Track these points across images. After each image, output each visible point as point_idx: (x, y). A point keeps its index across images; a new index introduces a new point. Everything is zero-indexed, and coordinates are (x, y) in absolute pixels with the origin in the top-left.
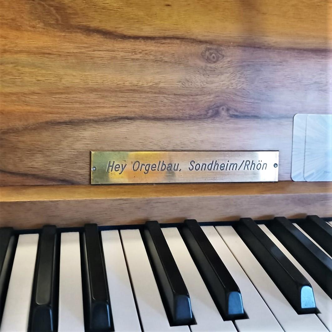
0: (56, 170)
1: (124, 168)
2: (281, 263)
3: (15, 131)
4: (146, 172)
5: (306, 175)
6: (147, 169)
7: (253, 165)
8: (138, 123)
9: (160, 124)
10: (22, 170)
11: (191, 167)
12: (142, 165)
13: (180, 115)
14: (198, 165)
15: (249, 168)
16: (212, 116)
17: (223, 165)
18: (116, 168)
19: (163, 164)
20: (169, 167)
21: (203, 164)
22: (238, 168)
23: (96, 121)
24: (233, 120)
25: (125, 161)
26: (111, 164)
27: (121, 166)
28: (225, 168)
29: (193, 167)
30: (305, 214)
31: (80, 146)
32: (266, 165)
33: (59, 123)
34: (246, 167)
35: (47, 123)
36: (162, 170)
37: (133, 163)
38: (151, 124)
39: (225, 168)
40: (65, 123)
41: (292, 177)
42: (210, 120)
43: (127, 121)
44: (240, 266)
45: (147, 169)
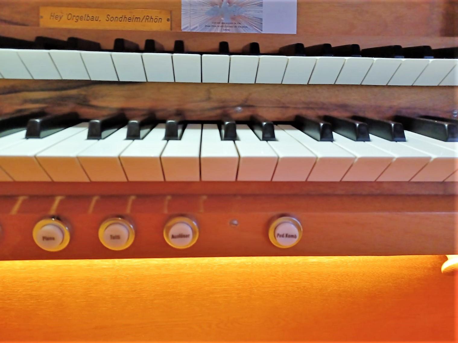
0: (18, 18)
4: (76, 21)
5: (192, 28)
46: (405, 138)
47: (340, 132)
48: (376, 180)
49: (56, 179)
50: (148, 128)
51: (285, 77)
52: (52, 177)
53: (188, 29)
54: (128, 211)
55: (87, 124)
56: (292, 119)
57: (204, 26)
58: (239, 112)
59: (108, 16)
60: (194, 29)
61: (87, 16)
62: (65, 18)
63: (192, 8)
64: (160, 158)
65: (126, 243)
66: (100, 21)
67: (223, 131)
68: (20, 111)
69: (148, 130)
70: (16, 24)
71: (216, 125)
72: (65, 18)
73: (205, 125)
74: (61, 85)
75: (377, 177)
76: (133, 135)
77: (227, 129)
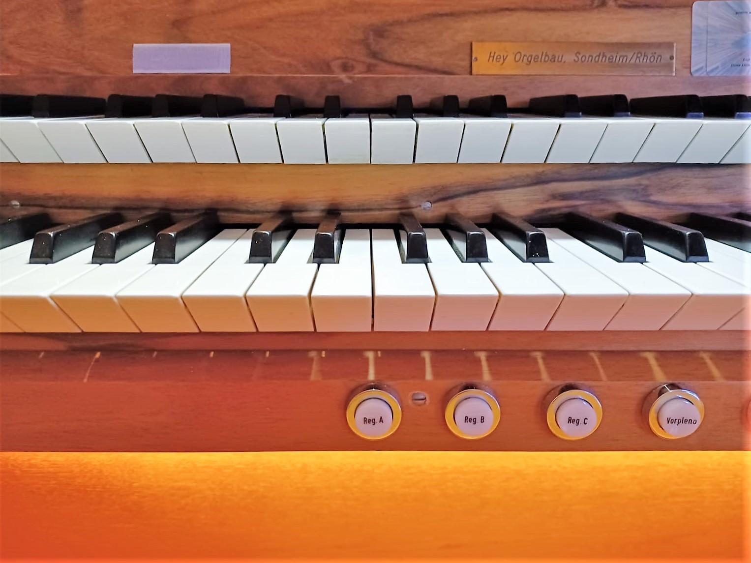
0: (437, 62)
1: (506, 58)
2: (492, 399)
3: (399, 23)
4: (528, 63)
5: (709, 69)
6: (529, 59)
7: (646, 58)
8: (518, 14)
9: (541, 15)
10: (407, 61)
11: (576, 59)
12: (524, 56)
13: (564, 6)
14: (519, 54)
15: (641, 60)
16: (598, 7)
17: (611, 58)
18: (497, 58)
19: (546, 55)
20: (552, 59)
21: (590, 56)
22: (628, 61)
23: (476, 13)
24: (620, 10)
25: (507, 52)
26: (492, 55)
27: (502, 57)
28: (539, 60)
29: (578, 59)
30: (741, 117)
31: (460, 38)
32: (519, 54)
33: (441, 15)
34: (638, 59)
35: (429, 15)
36: (545, 61)
37: (515, 54)
38: (532, 15)
39: (539, 60)
40: (446, 15)
41: (692, 71)
42: (596, 11)
43: (507, 12)
44: (733, 144)
45: (529, 59)
46: (645, 256)
47: (720, 241)
48: (718, 329)
49: (145, 330)
50: (280, 239)
51: (601, 144)
52: (140, 328)
53: (703, 70)
54: (371, 376)
55: (314, 232)
56: (487, 221)
57: (730, 65)
58: (427, 210)
59: (578, 54)
60: (712, 71)
61: (544, 54)
62: (510, 58)
63: (709, 37)
64: (245, 297)
65: (385, 430)
66: (565, 62)
67: (404, 244)
68: (543, 210)
69: (200, 242)
70: (435, 71)
71: (391, 232)
72: (510, 58)
73: (348, 231)
74: (642, 168)
75: (720, 325)
76: (165, 255)
77: (412, 241)
